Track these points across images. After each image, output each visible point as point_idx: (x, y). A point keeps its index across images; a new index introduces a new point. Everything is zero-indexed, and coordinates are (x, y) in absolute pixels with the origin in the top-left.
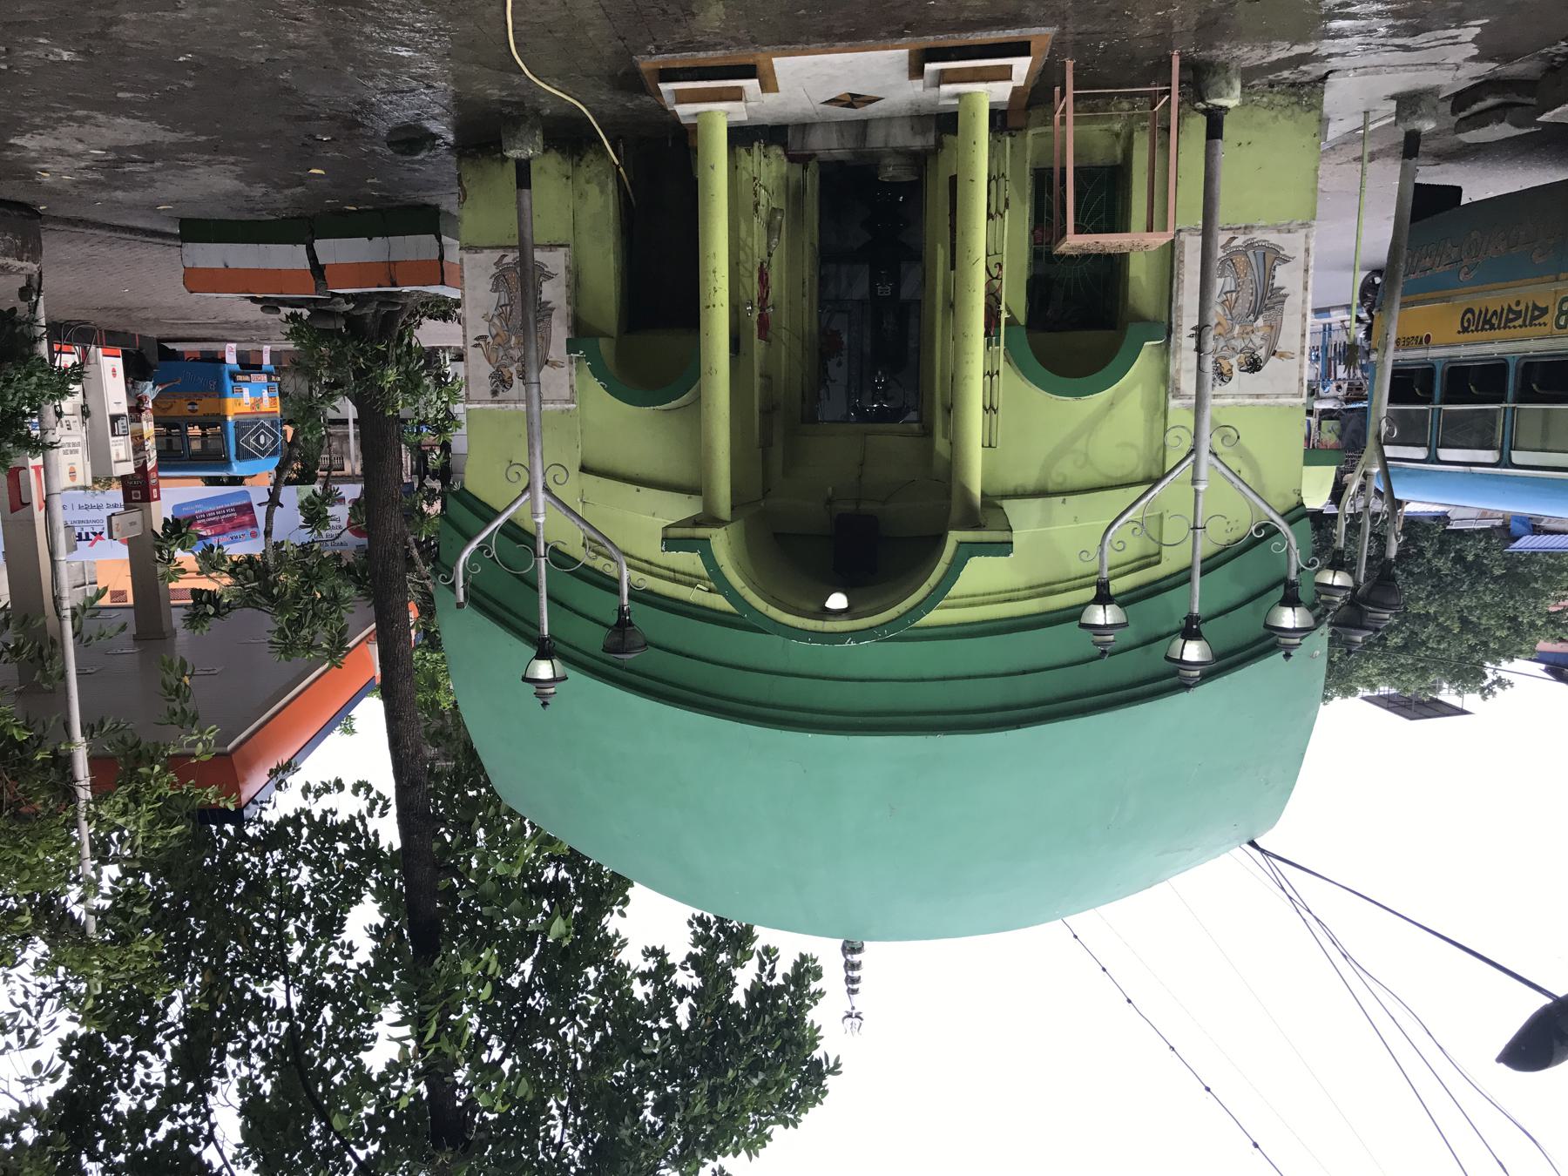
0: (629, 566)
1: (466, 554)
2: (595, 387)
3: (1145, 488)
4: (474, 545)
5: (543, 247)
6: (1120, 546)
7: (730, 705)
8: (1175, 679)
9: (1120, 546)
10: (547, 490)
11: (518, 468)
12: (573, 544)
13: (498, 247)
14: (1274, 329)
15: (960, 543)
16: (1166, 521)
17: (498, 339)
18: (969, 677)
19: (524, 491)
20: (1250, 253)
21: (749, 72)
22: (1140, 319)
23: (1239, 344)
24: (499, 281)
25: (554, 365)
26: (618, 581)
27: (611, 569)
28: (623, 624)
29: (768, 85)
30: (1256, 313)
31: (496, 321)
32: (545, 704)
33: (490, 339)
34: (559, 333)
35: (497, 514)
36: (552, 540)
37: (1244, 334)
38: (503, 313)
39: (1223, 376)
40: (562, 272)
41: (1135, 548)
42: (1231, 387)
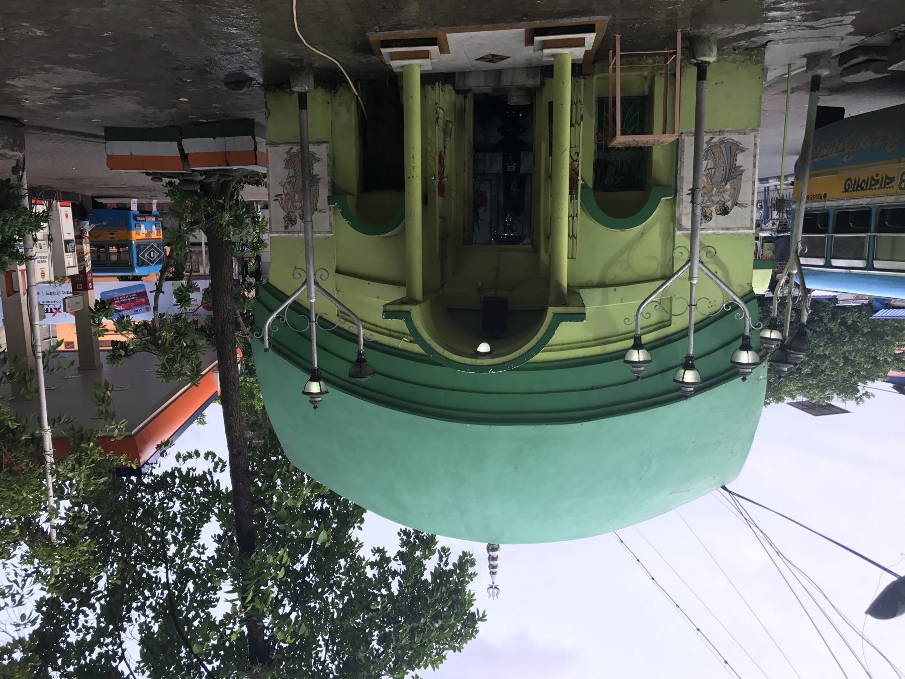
0: (364, 327)
1: (270, 320)
2: (344, 224)
3: (661, 282)
4: (274, 315)
5: (314, 143)
6: (648, 316)
7: (439, 410)
8: (679, 393)
9: (648, 316)
10: (316, 283)
11: (300, 271)
12: (332, 315)
13: (288, 143)
14: (736, 190)
15: (555, 314)
16: (674, 302)
20: (722, 146)
21: (432, 42)
22: (659, 184)
23: (716, 199)
24: (289, 162)
25: (320, 211)
26: (358, 336)
27: (353, 329)
28: (360, 361)
29: (444, 49)
30: (726, 180)
31: (287, 186)
32: (315, 407)
33: (283, 196)
34: (324, 192)
35: (288, 297)
36: (320, 313)
37: (719, 193)
38: (291, 181)
39: (707, 217)
40: (325, 158)
41: (655, 317)
42: (711, 223)
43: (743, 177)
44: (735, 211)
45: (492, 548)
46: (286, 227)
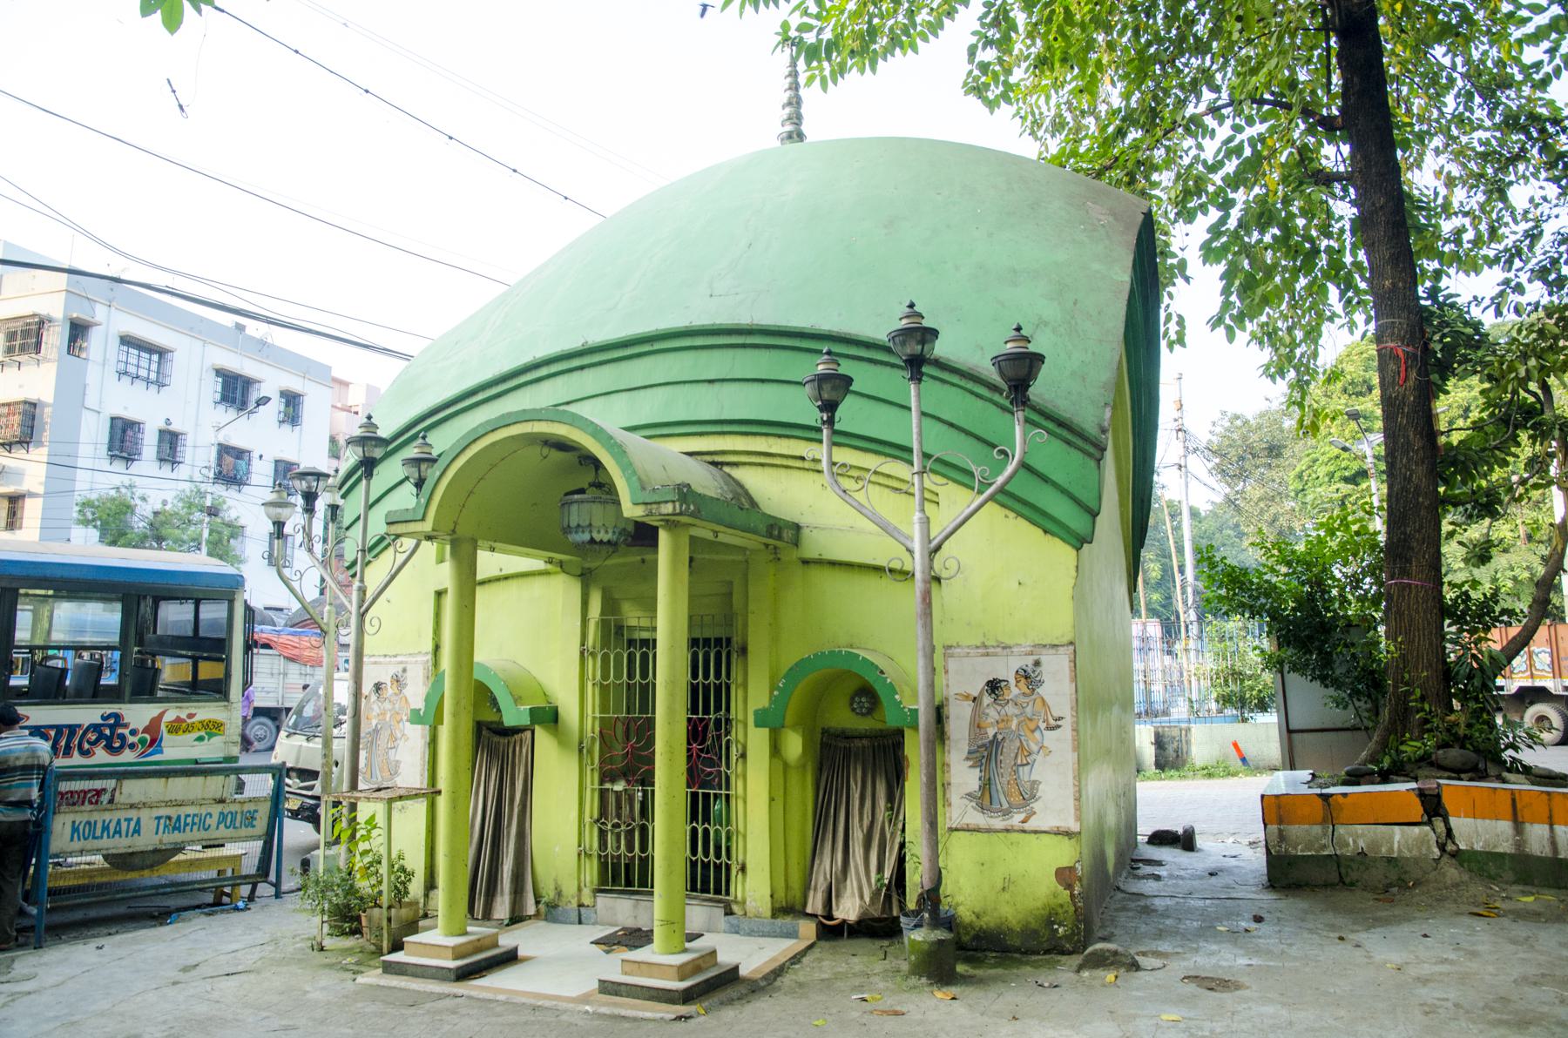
15: (423, 519)
17: (1032, 726)
18: (763, 381)
19: (938, 548)
20: (1005, 806)
23: (387, 705)
31: (1034, 748)
33: (1043, 726)
37: (1005, 720)
38: (1025, 756)
43: (966, 749)
44: (977, 686)
45: (796, 136)
46: (404, 670)
